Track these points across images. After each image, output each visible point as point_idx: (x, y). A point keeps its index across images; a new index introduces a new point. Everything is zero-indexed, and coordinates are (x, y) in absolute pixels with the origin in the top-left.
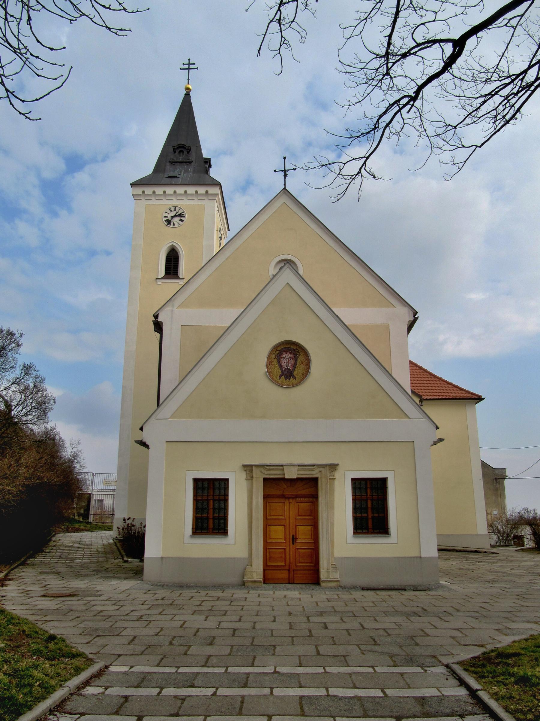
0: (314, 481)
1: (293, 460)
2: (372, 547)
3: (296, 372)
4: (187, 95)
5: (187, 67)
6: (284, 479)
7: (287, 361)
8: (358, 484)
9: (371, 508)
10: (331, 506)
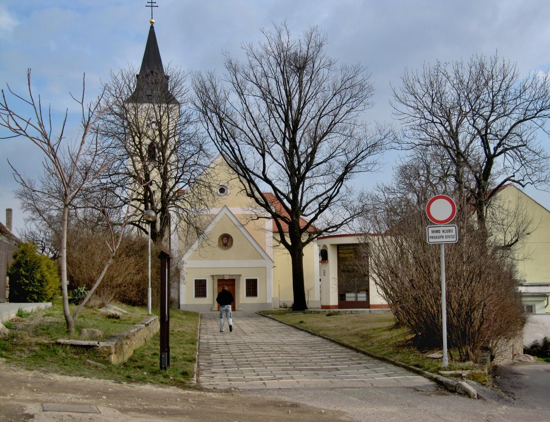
0: (233, 280)
1: (227, 273)
2: (252, 300)
3: (228, 244)
4: (152, 27)
5: (150, 4)
6: (224, 280)
7: (225, 241)
8: (248, 281)
9: (252, 288)
10: (239, 288)
